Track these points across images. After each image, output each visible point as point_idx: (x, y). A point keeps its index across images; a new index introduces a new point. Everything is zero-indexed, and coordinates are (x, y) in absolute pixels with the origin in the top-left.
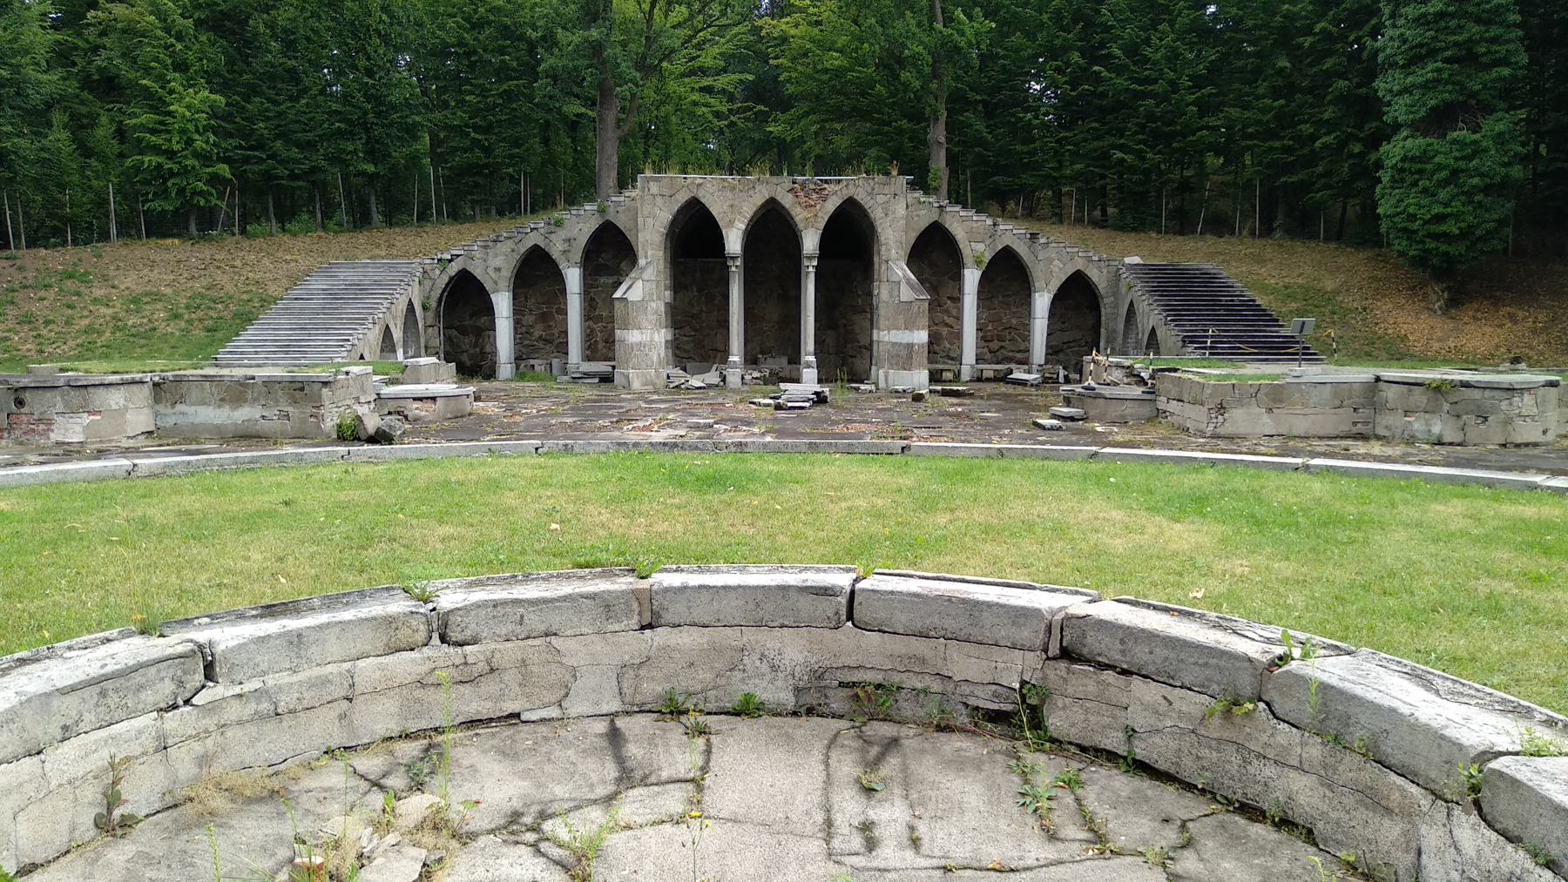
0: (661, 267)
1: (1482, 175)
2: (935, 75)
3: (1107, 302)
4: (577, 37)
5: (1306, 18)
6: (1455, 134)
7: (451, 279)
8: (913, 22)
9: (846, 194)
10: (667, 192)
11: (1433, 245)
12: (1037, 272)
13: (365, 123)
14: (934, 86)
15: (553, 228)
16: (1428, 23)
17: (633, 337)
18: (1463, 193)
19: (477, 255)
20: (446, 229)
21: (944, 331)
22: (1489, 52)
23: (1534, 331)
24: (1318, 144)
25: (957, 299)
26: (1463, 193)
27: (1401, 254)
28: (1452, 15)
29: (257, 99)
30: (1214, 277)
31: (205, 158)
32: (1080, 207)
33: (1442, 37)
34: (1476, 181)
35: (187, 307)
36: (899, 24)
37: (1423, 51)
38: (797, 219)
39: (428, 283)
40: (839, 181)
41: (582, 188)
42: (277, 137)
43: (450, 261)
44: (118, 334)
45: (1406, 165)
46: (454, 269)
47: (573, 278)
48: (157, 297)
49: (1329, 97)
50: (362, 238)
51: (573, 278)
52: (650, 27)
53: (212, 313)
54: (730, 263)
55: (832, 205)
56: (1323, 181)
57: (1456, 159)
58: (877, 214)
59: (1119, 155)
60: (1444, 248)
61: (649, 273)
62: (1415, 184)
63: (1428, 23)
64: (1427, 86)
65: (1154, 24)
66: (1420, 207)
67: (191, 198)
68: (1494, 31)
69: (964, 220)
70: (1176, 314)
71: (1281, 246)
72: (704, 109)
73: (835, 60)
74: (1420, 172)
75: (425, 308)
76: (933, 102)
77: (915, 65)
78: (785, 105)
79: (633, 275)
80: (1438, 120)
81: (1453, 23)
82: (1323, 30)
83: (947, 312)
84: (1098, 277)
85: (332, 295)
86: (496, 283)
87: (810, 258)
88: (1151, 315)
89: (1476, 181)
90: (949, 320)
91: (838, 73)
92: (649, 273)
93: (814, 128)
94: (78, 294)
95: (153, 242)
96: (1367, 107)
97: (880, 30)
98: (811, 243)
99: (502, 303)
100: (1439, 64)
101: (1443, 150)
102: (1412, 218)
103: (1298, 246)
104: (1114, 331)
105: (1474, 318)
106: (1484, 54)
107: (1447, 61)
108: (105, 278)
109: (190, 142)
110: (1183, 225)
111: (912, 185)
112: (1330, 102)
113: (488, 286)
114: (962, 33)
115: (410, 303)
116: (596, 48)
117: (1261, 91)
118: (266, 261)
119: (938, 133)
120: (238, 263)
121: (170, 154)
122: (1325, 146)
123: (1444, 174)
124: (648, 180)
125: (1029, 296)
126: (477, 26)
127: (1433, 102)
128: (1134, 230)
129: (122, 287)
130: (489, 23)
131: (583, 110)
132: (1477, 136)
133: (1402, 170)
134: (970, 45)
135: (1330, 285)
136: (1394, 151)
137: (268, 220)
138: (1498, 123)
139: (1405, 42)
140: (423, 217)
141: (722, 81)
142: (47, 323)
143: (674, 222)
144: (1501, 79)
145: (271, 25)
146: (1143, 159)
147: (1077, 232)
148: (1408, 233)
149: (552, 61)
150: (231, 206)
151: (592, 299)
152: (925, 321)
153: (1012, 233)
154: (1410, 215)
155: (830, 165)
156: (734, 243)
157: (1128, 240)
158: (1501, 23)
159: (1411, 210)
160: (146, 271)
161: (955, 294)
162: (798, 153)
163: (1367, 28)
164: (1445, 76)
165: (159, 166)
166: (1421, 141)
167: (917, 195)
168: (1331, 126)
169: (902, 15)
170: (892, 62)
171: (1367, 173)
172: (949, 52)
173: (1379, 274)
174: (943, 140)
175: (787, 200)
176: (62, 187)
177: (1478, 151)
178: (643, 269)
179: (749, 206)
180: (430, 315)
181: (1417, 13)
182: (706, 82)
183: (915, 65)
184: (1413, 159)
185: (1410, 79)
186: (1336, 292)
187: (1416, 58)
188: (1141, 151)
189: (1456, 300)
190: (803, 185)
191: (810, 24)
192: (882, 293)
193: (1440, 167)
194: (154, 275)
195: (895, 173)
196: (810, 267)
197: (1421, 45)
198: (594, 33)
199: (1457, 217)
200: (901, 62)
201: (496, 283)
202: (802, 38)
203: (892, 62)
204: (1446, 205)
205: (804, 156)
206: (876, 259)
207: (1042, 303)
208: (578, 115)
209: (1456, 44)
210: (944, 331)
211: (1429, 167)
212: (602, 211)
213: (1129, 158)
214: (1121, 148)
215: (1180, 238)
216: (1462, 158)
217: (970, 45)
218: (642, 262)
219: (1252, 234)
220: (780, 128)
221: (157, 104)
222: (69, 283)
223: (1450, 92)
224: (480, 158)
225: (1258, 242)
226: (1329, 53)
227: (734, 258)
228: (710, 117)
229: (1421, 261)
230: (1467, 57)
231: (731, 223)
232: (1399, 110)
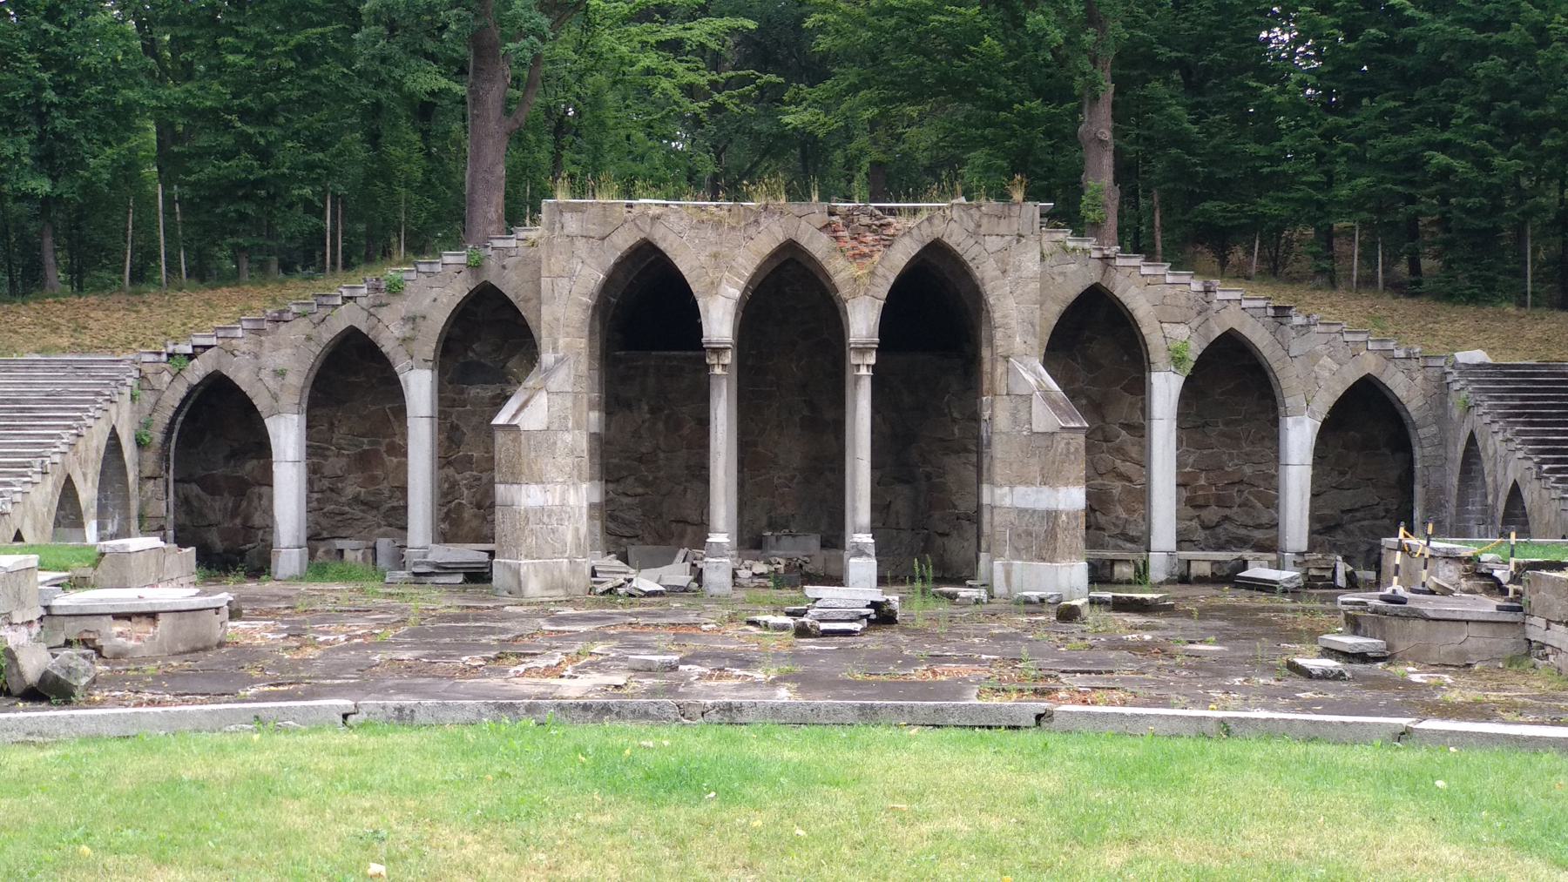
0: (583, 367)
7: (192, 389)
9: (928, 234)
10: (595, 230)
12: (1289, 378)
15: (384, 298)
20: (185, 298)
21: (1117, 487)
25: (1140, 430)
32: (1368, 257)
39: (148, 399)
40: (915, 211)
43: (191, 357)
46: (197, 371)
54: (711, 359)
55: (902, 254)
58: (986, 271)
59: (1440, 158)
75: (140, 444)
76: (1088, 67)
78: (815, 71)
79: (530, 382)
83: (1120, 451)
84: (1406, 387)
86: (275, 397)
87: (862, 351)
92: (562, 379)
93: (867, 115)
98: (863, 322)
104: (1441, 490)
111: (1053, 219)
113: (261, 402)
115: (114, 437)
119: (1099, 124)
124: (561, 209)
125: (1275, 422)
128: (1473, 299)
131: (443, 83)
146: (1486, 167)
151: (454, 428)
152: (1079, 468)
161: (1136, 418)
162: (838, 157)
167: (1060, 236)
174: (1107, 135)
175: (818, 246)
178: (549, 372)
180: (151, 457)
182: (671, 32)
190: (848, 218)
192: (998, 415)
196: (862, 369)
201: (275, 397)
205: (851, 164)
206: (986, 353)
210: (1117, 487)
212: (475, 267)
213: (1460, 165)
214: (1444, 147)
218: (547, 358)
227: (718, 351)
231: (714, 287)
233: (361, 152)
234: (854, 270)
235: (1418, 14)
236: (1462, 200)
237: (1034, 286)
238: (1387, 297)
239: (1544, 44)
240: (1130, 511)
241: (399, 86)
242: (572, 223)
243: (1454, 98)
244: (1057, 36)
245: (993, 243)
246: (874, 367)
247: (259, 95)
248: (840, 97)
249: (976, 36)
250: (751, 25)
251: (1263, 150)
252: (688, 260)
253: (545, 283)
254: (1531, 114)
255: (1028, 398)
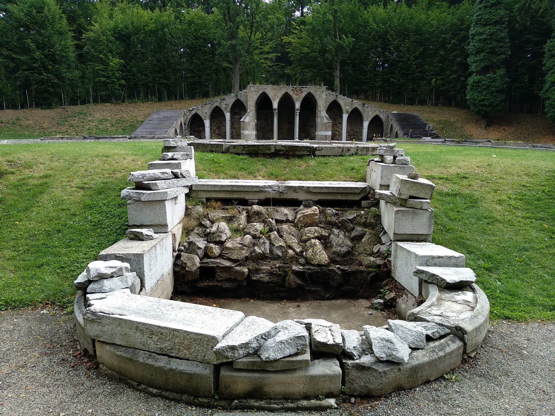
0: (254, 112)
1: (496, 87)
2: (336, 55)
3: (385, 124)
4: (229, 43)
5: (449, 39)
6: (488, 75)
7: (192, 115)
8: (330, 39)
9: (308, 91)
10: (256, 90)
11: (481, 108)
12: (365, 115)
13: (164, 69)
14: (336, 58)
15: (222, 101)
16: (482, 42)
17: (246, 132)
18: (490, 93)
19: (200, 108)
20: (187, 102)
21: (337, 133)
22: (499, 50)
23: (510, 134)
24: (451, 78)
25: (341, 124)
26: (490, 93)
27: (473, 111)
28: (489, 39)
29: (133, 61)
30: (417, 117)
31: (118, 79)
32: (381, 97)
33: (485, 46)
34: (494, 89)
35: (116, 123)
36: (325, 40)
37: (480, 50)
38: (294, 98)
39: (186, 117)
40: (306, 87)
41: (228, 90)
42: (139, 72)
43: (192, 110)
44: (98, 130)
45: (474, 84)
46: (193, 113)
47: (228, 116)
48: (107, 120)
49: (455, 63)
50: (163, 104)
51: (228, 116)
52: (250, 40)
53: (123, 125)
54: (274, 111)
55: (304, 94)
56: (453, 89)
57: (489, 82)
58: (317, 97)
59: (392, 79)
60: (484, 109)
61: (251, 114)
62: (476, 90)
63: (482, 42)
64: (481, 60)
65: (404, 39)
66: (478, 96)
67: (114, 91)
68: (501, 44)
69: (343, 99)
70: (403, 127)
71: (440, 108)
72: (265, 65)
73: (306, 50)
74: (478, 86)
75: (185, 124)
76: (335, 63)
77: (330, 52)
78: (290, 63)
79: (246, 114)
80: (484, 71)
81: (489, 42)
82: (454, 43)
83: (338, 127)
84: (383, 117)
85: (160, 120)
86: (205, 117)
87: (297, 110)
88: (397, 128)
89: (494, 89)
90: (339, 130)
91: (307, 54)
92: (251, 114)
93: (299, 71)
94: (84, 119)
95: (102, 104)
96: (466, 66)
97: (319, 41)
98: (298, 105)
99: (207, 123)
100: (484, 54)
101: (485, 79)
102: (475, 100)
103: (446, 109)
104: (387, 133)
105: (493, 130)
106: (498, 51)
107: (487, 53)
108: (91, 114)
109: (113, 74)
110: (411, 102)
111: (328, 89)
112: (456, 65)
113: (203, 118)
114: (344, 42)
115: (181, 123)
116: (233, 47)
117: (435, 61)
118: (136, 110)
119: (337, 73)
120: (128, 111)
121: (108, 77)
122: (454, 78)
123: (484, 87)
124: (251, 87)
125: (362, 122)
126: (197, 38)
127: (482, 66)
128: (397, 103)
129: (96, 117)
130: (201, 38)
131: (228, 65)
132: (495, 76)
133: (473, 86)
134: (347, 45)
135: (453, 120)
136: (471, 80)
137: (135, 98)
138: (502, 72)
139: (475, 47)
140: (181, 98)
141: (270, 56)
142: (77, 127)
143: (258, 99)
144: (502, 59)
145: (138, 39)
146: (399, 81)
147: (379, 104)
148: (475, 104)
149: (220, 50)
150: (125, 93)
151: (233, 122)
152: (331, 129)
153: (357, 104)
154: (475, 99)
155: (304, 82)
156: (275, 105)
157: (395, 106)
158: (503, 42)
159: (475, 98)
160: (102, 113)
161: (341, 122)
162: (294, 78)
163: (467, 42)
164: (486, 57)
165: (105, 81)
166: (478, 77)
167: (329, 92)
168: (455, 72)
169: (326, 37)
170: (323, 51)
171: (464, 86)
172: (340, 48)
173: (468, 117)
174: (338, 75)
175: (291, 93)
176: (77, 87)
177: (495, 80)
178: (249, 113)
179: (280, 94)
180: (186, 126)
181: (479, 38)
182: (266, 56)
183: (330, 52)
184: (476, 82)
185: (477, 58)
186: (454, 122)
187: (478, 52)
188: (399, 79)
189: (489, 124)
190: (296, 88)
191: (298, 38)
192: (318, 120)
193: (484, 85)
194: (105, 114)
195: (323, 85)
196: (297, 113)
197: (480, 48)
198: (234, 42)
199: (488, 99)
200: (326, 51)
201: (205, 117)
202: (296, 43)
203: (323, 51)
204: (485, 96)
205: (296, 80)
206: (317, 111)
207: (366, 124)
208: (226, 67)
209: (490, 48)
210: (337, 133)
211: (480, 84)
212: (236, 96)
213: (395, 81)
214: (393, 78)
215: (410, 106)
216: (491, 82)
217: (347, 45)
218: (249, 111)
219: (432, 105)
220: (289, 71)
221: (105, 63)
222: (81, 115)
223: (487, 62)
224: (198, 80)
225: (433, 107)
226: (455, 50)
227: (275, 110)
228: (267, 67)
229: (478, 113)
230: (493, 52)
231: (275, 99)
232: (473, 68)
233: (215, 77)
234: (296, 97)
235: (389, 55)
236: (47, 74)
237: (325, 100)
238: (383, 103)
239: (409, 61)
240: (339, 137)
241: (221, 65)
242: (252, 89)
243: (395, 69)
244: (330, 58)
245: (318, 93)
246: (299, 113)
247: (199, 67)
248: (294, 68)
249: (317, 58)
250: (279, 55)
251: (364, 78)
252: (270, 96)
253: (248, 99)
254: (407, 72)
255: (323, 117)
